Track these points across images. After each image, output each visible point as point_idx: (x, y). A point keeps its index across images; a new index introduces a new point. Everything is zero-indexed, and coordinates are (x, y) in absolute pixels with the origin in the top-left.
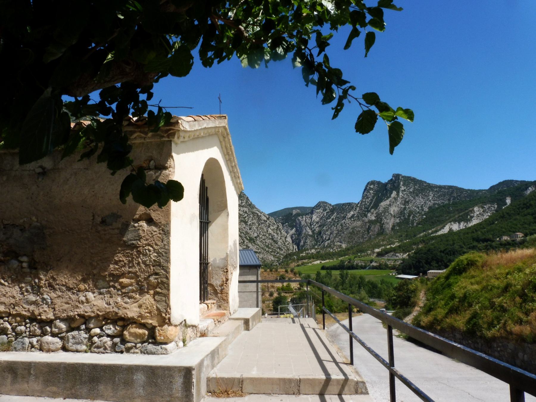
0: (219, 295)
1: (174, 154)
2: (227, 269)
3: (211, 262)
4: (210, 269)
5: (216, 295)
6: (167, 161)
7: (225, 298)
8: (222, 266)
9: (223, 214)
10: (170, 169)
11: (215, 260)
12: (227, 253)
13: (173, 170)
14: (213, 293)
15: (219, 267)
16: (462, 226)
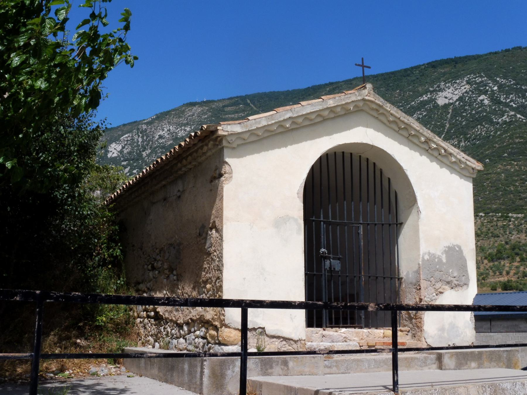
0: (414, 320)
1: (227, 160)
2: (420, 286)
3: (404, 277)
4: (404, 286)
5: (410, 321)
6: (222, 168)
7: (419, 325)
8: (414, 281)
9: (413, 211)
10: (226, 175)
11: (408, 274)
12: (419, 264)
13: (230, 176)
14: (408, 318)
15: (411, 283)
16: (450, 114)
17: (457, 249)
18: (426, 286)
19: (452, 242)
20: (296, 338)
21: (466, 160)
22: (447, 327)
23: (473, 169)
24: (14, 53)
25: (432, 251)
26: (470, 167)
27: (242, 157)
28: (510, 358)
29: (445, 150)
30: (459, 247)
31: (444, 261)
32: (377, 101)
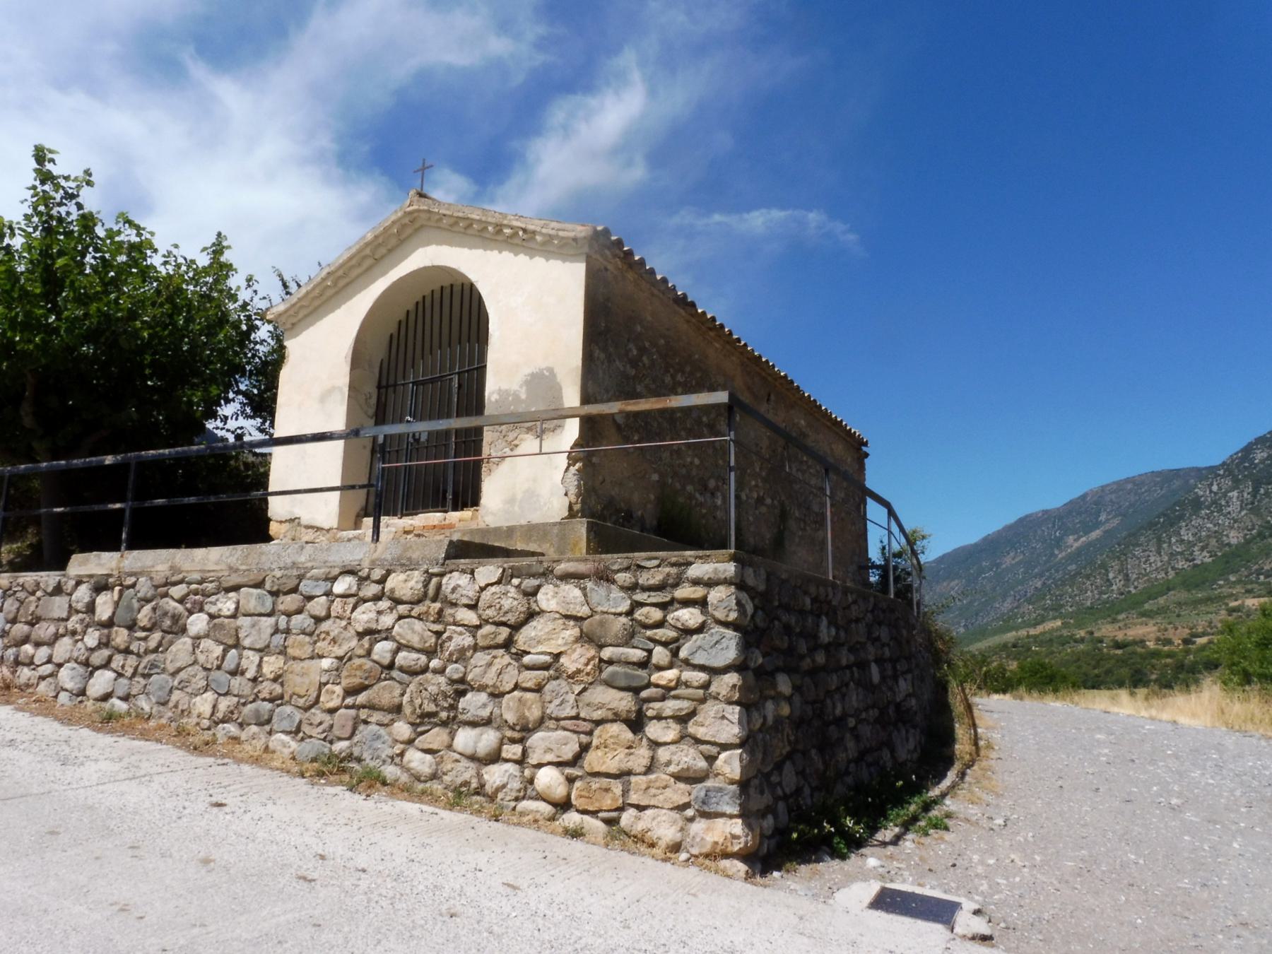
17: (547, 374)
18: (490, 440)
19: (540, 364)
20: (327, 527)
21: (558, 230)
22: (519, 496)
23: (575, 240)
24: (783, 208)
25: (504, 386)
26: (567, 238)
27: (298, 335)
28: (564, 535)
29: (525, 230)
30: (551, 370)
31: (523, 396)
32: (422, 208)
